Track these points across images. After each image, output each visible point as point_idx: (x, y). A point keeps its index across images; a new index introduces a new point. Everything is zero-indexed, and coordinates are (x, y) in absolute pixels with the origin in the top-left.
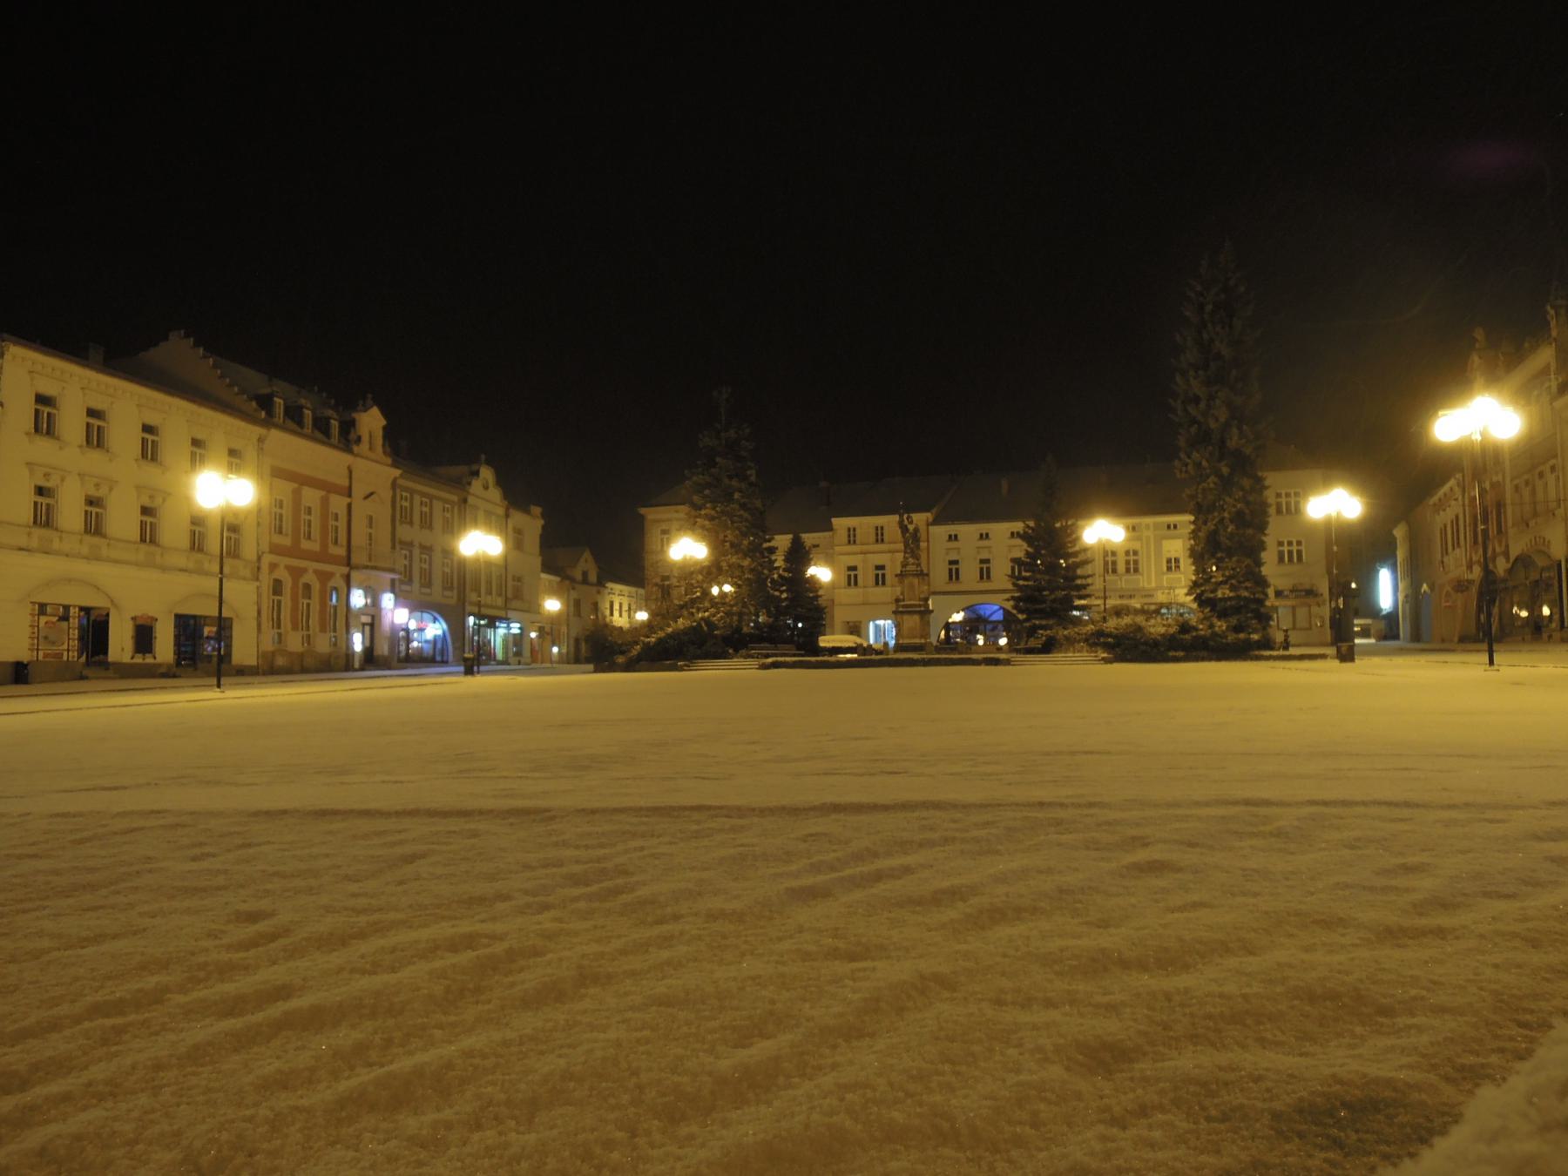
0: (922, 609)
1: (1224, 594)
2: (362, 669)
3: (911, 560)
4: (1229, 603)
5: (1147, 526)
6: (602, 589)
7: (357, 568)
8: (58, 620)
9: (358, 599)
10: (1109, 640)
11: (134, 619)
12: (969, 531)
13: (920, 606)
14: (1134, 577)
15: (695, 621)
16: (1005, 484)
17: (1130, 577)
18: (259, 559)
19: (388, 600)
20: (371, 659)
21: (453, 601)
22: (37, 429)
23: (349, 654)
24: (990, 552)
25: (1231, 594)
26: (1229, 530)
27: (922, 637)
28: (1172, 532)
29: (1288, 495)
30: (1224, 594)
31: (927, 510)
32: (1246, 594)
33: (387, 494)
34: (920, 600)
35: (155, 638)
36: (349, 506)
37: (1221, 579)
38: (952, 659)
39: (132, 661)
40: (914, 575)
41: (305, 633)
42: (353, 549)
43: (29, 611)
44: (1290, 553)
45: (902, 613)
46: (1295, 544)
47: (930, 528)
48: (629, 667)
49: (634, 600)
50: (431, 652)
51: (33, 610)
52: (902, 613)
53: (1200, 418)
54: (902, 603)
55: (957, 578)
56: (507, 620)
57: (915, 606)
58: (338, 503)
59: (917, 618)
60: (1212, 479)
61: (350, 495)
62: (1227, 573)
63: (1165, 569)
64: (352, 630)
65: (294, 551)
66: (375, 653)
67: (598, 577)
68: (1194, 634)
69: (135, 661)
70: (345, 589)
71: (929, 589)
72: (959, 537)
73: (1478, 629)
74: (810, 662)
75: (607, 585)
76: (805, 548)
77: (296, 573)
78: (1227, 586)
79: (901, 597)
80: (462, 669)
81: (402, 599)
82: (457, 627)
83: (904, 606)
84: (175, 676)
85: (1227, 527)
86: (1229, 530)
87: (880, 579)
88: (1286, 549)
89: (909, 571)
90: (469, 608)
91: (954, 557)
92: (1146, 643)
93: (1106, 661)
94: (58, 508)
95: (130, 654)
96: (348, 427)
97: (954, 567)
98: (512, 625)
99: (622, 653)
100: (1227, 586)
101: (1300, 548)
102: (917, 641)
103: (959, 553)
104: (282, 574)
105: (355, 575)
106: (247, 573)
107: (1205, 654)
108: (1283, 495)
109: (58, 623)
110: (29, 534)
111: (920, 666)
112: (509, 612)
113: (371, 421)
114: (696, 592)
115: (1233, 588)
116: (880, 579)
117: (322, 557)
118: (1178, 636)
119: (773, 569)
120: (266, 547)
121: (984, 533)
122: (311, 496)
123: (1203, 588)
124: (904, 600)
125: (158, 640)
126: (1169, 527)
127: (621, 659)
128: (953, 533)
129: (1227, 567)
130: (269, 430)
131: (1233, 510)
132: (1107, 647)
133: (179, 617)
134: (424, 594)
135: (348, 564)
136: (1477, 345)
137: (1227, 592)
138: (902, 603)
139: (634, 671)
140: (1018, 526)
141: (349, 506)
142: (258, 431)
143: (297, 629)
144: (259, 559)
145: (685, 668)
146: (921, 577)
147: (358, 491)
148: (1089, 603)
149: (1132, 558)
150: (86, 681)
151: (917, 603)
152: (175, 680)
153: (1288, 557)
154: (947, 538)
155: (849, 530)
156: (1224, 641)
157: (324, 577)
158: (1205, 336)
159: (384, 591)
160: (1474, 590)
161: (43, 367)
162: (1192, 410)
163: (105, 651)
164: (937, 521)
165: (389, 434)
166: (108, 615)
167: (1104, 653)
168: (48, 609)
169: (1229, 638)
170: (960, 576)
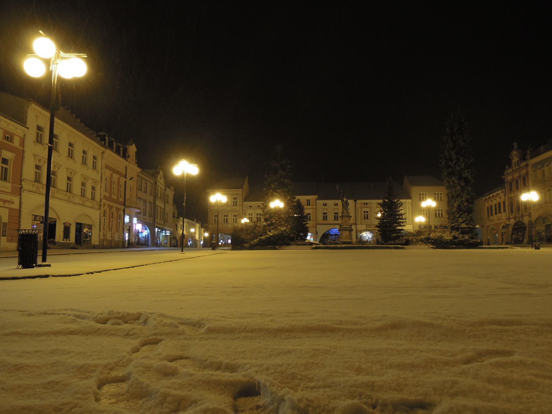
0: (350, 229)
1: (464, 226)
2: (128, 248)
3: (345, 211)
4: (466, 229)
5: (374, 203)
6: (178, 219)
7: (128, 207)
8: (40, 223)
9: (127, 219)
10: (432, 241)
11: (64, 223)
12: (330, 203)
13: (349, 228)
14: (367, 220)
15: (281, 231)
16: (338, 187)
17: (365, 220)
18: (101, 201)
19: (135, 220)
20: (130, 245)
21: (151, 222)
22: (37, 141)
23: (124, 241)
24: (338, 210)
25: (467, 226)
26: (465, 204)
27: (349, 239)
28: (366, 206)
29: (423, 194)
30: (464, 226)
31: (315, 194)
32: (471, 226)
33: (136, 178)
34: (349, 226)
35: (70, 232)
36: (125, 182)
37: (462, 221)
38: (383, 247)
39: (63, 242)
40: (347, 217)
41: (111, 232)
42: (126, 199)
43: (31, 219)
44: (439, 213)
45: (343, 230)
46: (437, 211)
47: (317, 201)
48: (252, 248)
49: (188, 224)
50: (144, 242)
51: (33, 218)
52: (343, 230)
53: (453, 166)
54: (342, 227)
55: (227, 222)
56: (166, 230)
57: (348, 228)
58: (123, 180)
59: (348, 232)
60: (458, 187)
61: (126, 178)
62: (464, 219)
63: (363, 218)
64: (125, 232)
65: (109, 199)
66: (130, 241)
67: (178, 216)
68: (459, 239)
69: (65, 241)
70: (123, 215)
71: (316, 222)
72: (327, 204)
73: (512, 240)
74: (330, 247)
75: (180, 218)
76: (302, 206)
77: (110, 207)
78: (465, 224)
79: (342, 224)
80: (211, 248)
81: (139, 221)
82: (152, 232)
83: (343, 228)
84: (75, 249)
85: (464, 203)
86: (465, 204)
87: (235, 221)
88: (437, 212)
89: (345, 215)
90: (156, 225)
91: (325, 211)
92: (443, 242)
93: (433, 248)
94: (42, 174)
95: (62, 239)
96: (125, 150)
97: (325, 215)
98: (167, 232)
99: (246, 243)
100: (465, 224)
101: (442, 212)
102: (348, 240)
103: (327, 210)
104: (107, 208)
105: (127, 210)
106: (97, 207)
107: (462, 246)
108: (422, 194)
109: (40, 224)
110: (33, 185)
111: (372, 249)
112: (165, 227)
113: (132, 149)
114: (273, 220)
115: (466, 224)
116: (235, 221)
117: (116, 202)
118: (453, 240)
119: (397, 212)
120: (102, 197)
121: (336, 203)
122: (115, 176)
123: (455, 224)
124: (343, 226)
125: (71, 233)
126: (365, 204)
127: (246, 245)
128: (325, 203)
129: (464, 217)
130: (106, 149)
131: (466, 198)
132: (433, 244)
133: (77, 224)
134: (144, 218)
135: (124, 205)
136: (515, 148)
137: (465, 225)
138: (342, 227)
139: (252, 250)
140: (381, 201)
141: (125, 182)
142: (103, 149)
143: (117, 232)
144: (101, 201)
145: (279, 249)
146: (349, 218)
147: (128, 176)
148: (402, 228)
149: (259, 216)
150: (50, 250)
151: (348, 227)
152: (75, 250)
153: (441, 215)
154: (323, 205)
155: (307, 200)
156: (470, 242)
157: (118, 209)
158: (455, 138)
159: (134, 217)
160: (511, 228)
161: (40, 114)
162: (450, 163)
163: (54, 237)
164: (320, 198)
165: (138, 154)
166: (56, 221)
167: (431, 245)
168: (37, 218)
169: (471, 241)
170: (327, 219)
